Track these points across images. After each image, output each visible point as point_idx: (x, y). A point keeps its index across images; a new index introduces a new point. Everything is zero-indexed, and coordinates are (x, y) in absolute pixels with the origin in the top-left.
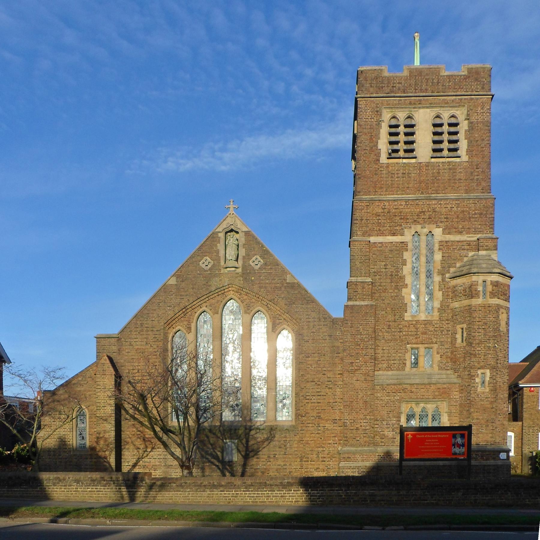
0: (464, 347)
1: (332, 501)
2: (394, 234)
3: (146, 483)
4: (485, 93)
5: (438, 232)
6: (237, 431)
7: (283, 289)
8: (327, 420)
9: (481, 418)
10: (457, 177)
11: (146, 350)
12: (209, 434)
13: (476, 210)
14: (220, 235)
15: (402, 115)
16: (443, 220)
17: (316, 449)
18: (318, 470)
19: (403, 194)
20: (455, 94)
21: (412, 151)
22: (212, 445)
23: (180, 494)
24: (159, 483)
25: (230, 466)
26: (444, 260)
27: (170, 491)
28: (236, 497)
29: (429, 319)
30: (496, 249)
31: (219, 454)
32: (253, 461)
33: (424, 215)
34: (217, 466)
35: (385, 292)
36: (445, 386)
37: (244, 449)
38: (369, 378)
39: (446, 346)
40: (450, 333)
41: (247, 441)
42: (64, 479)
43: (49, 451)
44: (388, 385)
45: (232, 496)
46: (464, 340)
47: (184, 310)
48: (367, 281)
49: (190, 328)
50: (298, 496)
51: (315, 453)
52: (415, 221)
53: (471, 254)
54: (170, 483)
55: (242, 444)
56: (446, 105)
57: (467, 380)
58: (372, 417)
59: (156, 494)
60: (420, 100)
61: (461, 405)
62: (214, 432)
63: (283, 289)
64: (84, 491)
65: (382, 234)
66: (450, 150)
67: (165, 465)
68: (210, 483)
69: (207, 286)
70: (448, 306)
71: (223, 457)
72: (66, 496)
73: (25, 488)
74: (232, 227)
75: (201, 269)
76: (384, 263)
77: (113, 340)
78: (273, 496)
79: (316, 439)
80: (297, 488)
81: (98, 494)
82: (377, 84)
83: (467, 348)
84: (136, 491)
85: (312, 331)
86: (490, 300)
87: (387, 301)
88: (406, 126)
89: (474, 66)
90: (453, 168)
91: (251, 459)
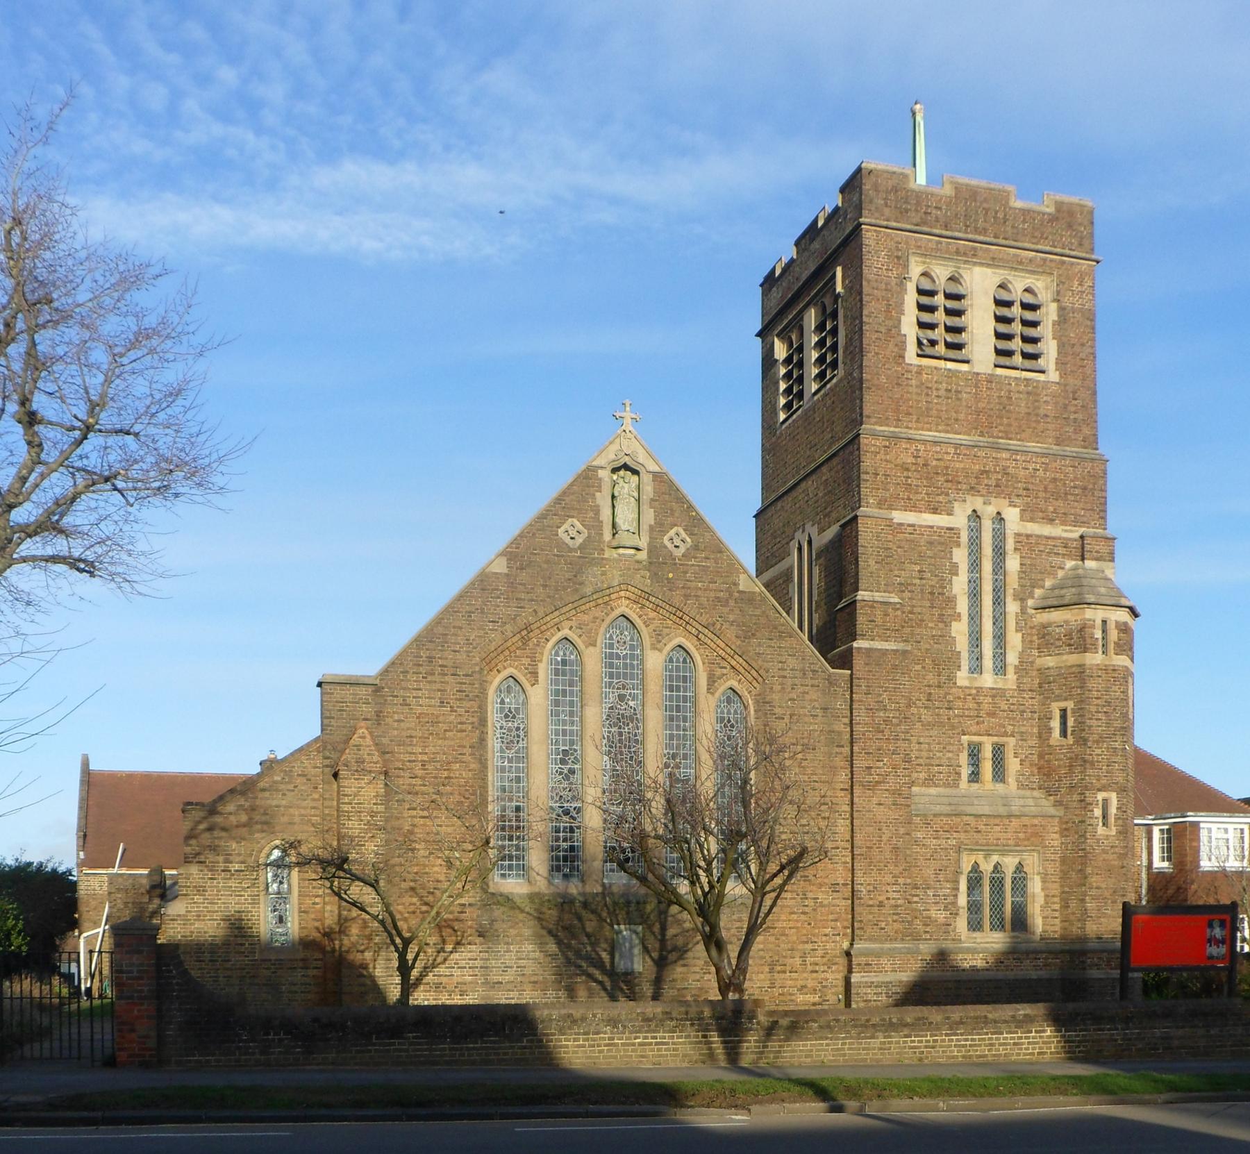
0: (1070, 747)
1: (1100, 1051)
2: (935, 511)
3: (758, 1023)
4: (1084, 255)
5: (1012, 515)
6: (641, 906)
7: (732, 603)
8: (821, 885)
9: (1103, 886)
10: (1042, 412)
11: (441, 719)
12: (584, 913)
13: (1076, 479)
15: (941, 273)
16: (1021, 492)
17: (801, 947)
18: (805, 990)
19: (947, 432)
20: (1033, 247)
21: (959, 347)
22: (588, 936)
23: (827, 1045)
24: (784, 1022)
25: (627, 983)
26: (1024, 572)
27: (807, 1039)
29: (1000, 686)
30: (1113, 560)
31: (604, 955)
32: (678, 971)
33: (988, 478)
34: (600, 983)
35: (919, 626)
36: (1036, 821)
37: (657, 945)
38: (902, 798)
40: (1036, 716)
41: (663, 929)
42: (583, 1019)
44: (935, 815)
45: (926, 1047)
46: (1069, 732)
47: (524, 633)
48: (892, 600)
49: (535, 674)
51: (797, 954)
53: (1070, 564)
54: (807, 1022)
55: (653, 933)
56: (1018, 265)
58: (909, 881)
60: (975, 249)
61: (1063, 860)
62: (593, 907)
63: (732, 603)
64: (628, 1045)
65: (914, 508)
66: (949, 346)
67: (486, 983)
68: (884, 1020)
69: (575, 583)
70: (1032, 663)
71: (612, 962)
72: (588, 1058)
73: (492, 1042)
74: (627, 459)
75: (561, 545)
76: (918, 568)
77: (362, 691)
78: (1000, 1045)
79: (799, 925)
81: (659, 1050)
84: (740, 1042)
86: (1115, 657)
87: (924, 646)
88: (948, 296)
90: (1034, 392)
91: (670, 968)
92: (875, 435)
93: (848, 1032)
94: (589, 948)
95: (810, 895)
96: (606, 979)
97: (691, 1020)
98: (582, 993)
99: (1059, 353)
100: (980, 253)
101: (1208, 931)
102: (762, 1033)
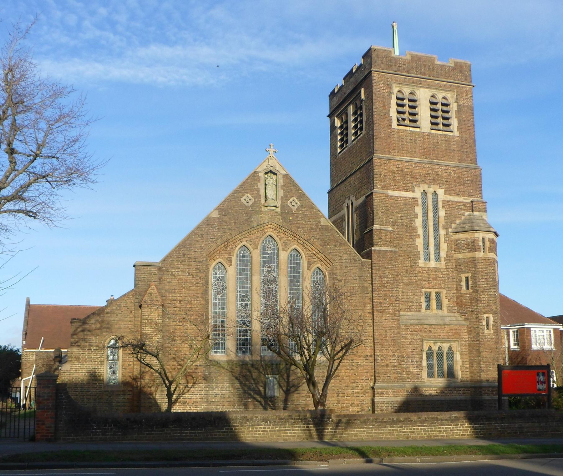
3: (332, 421)
4: (467, 83)
5: (441, 192)
6: (278, 366)
7: (318, 230)
8: (360, 356)
10: (452, 148)
11: (188, 281)
13: (468, 177)
14: (260, 174)
15: (406, 91)
16: (444, 182)
17: (351, 385)
18: (353, 405)
19: (411, 157)
22: (254, 380)
23: (364, 431)
24: (344, 420)
25: (271, 401)
27: (355, 428)
28: (413, 432)
29: (438, 266)
30: (486, 212)
31: (261, 389)
34: (260, 402)
35: (401, 240)
36: (456, 327)
37: (285, 384)
38: (395, 317)
39: (453, 292)
40: (455, 280)
41: (288, 377)
42: (252, 419)
43: (76, 386)
44: (411, 325)
45: (410, 432)
46: (470, 286)
47: (226, 243)
48: (389, 229)
50: (464, 430)
52: (423, 181)
53: (467, 213)
54: (355, 420)
55: (284, 379)
56: (439, 88)
57: (475, 323)
58: (400, 354)
59: (342, 432)
60: (421, 81)
61: (470, 345)
62: (256, 366)
63: (318, 230)
64: (272, 431)
65: (398, 189)
66: (411, 121)
67: (207, 402)
68: (390, 419)
70: (452, 256)
72: (254, 437)
73: (209, 429)
74: (271, 169)
77: (153, 269)
78: (444, 431)
79: (350, 375)
80: (463, 422)
81: (286, 433)
82: (387, 62)
83: (474, 295)
84: (324, 429)
85: (345, 271)
89: (459, 60)
90: (448, 140)
91: (292, 394)
92: (379, 158)
93: (374, 425)
94: (254, 386)
95: (355, 361)
96: (262, 400)
97: (301, 419)
98: (251, 407)
99: (458, 124)
100: (423, 83)
101: (537, 377)
102: (334, 425)
